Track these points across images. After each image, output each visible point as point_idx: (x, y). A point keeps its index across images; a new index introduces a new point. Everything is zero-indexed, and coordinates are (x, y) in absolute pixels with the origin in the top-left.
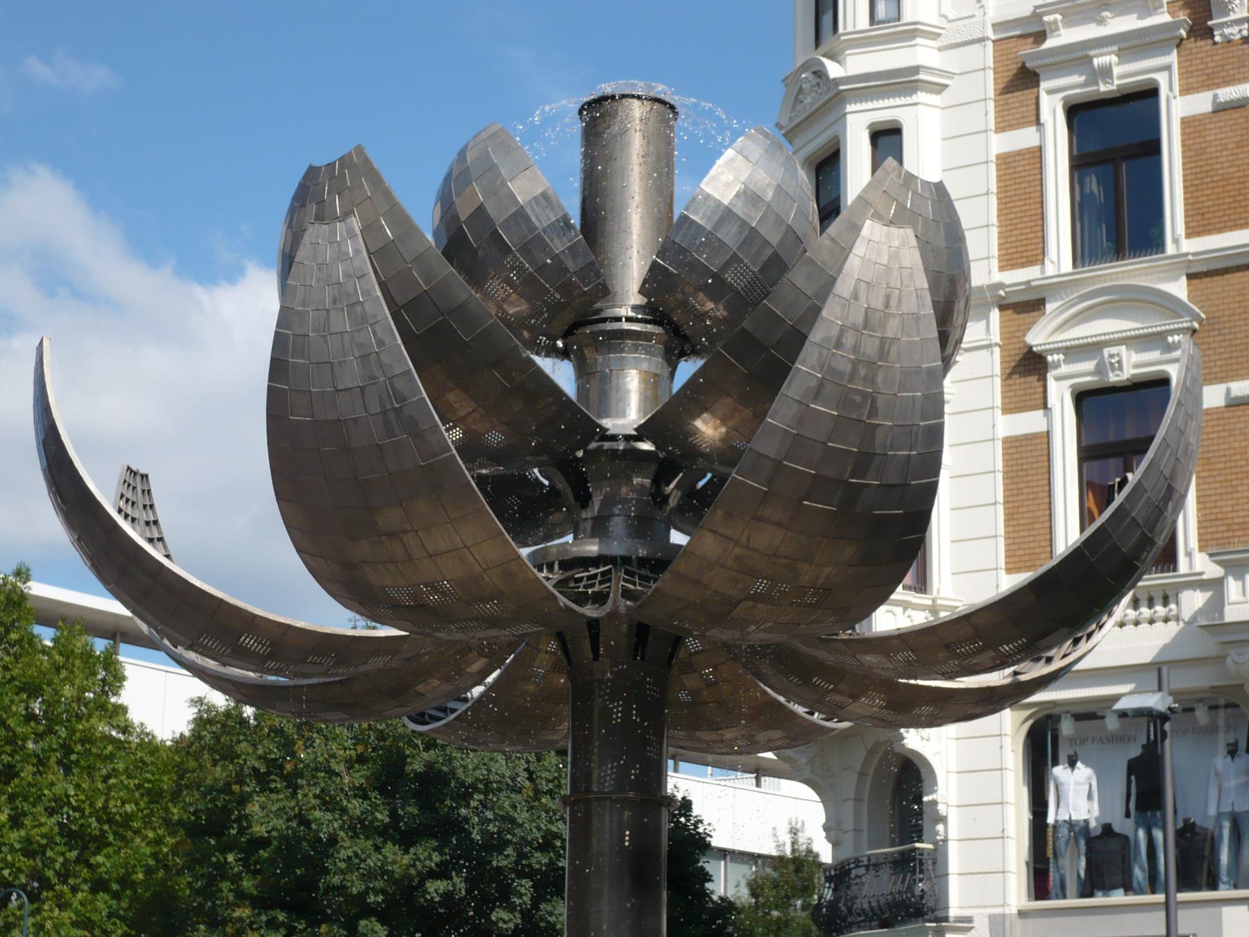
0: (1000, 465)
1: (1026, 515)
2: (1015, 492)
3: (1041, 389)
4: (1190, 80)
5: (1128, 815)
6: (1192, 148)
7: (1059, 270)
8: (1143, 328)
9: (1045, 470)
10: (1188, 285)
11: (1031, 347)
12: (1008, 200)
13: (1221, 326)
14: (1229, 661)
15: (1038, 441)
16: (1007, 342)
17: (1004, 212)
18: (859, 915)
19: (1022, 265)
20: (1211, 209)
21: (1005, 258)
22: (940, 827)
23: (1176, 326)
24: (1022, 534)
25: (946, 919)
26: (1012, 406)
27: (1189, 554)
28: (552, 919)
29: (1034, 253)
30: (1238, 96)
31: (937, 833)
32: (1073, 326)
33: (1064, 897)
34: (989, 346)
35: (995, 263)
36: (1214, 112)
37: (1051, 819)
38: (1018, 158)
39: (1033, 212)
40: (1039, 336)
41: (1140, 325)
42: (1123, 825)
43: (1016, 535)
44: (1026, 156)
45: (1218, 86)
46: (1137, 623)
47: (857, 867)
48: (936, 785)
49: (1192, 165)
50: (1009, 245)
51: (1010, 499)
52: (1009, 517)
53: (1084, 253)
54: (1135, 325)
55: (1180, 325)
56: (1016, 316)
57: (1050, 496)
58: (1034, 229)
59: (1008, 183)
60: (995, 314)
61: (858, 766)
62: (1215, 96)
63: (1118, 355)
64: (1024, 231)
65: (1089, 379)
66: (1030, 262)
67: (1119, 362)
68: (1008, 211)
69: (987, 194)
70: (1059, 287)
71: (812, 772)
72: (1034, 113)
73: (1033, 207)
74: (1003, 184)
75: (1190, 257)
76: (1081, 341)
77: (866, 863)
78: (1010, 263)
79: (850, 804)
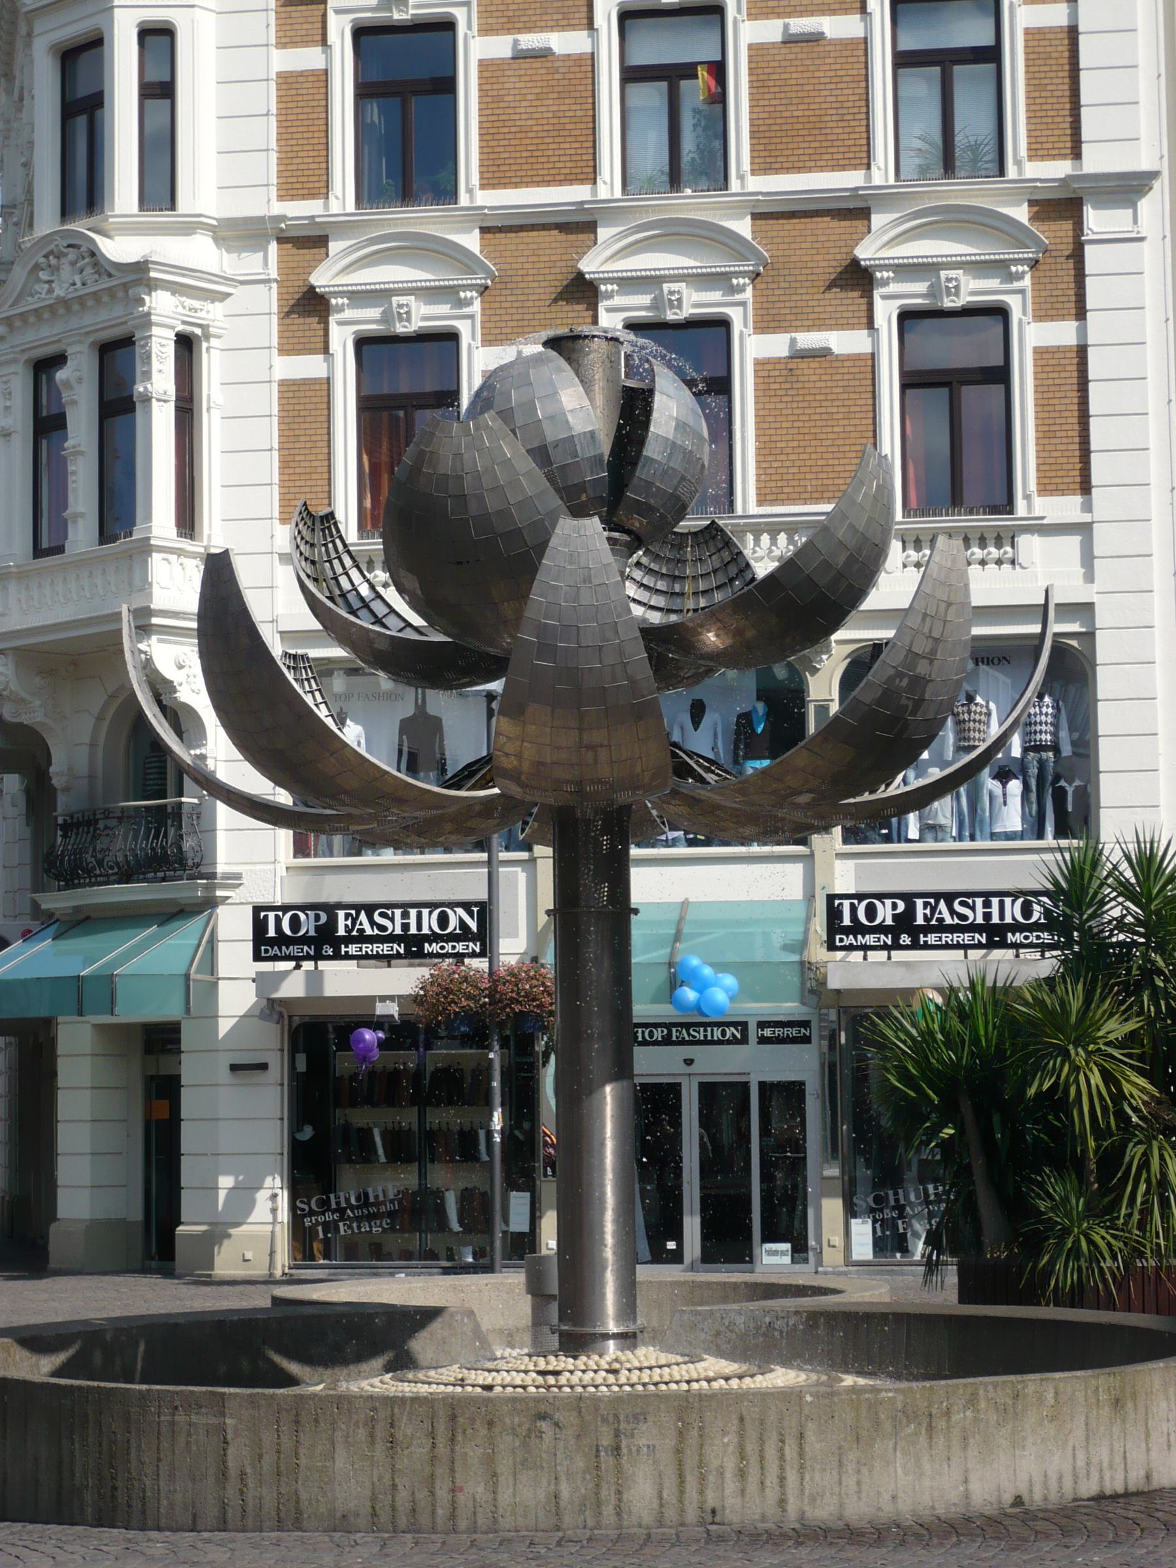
0: (275, 410)
1: (303, 464)
2: (291, 439)
3: (321, 333)
4: (490, 21)
6: (490, 93)
7: (344, 208)
8: (434, 281)
9: (324, 419)
10: (481, 239)
11: (312, 288)
12: (289, 124)
13: (514, 286)
15: (317, 387)
16: (285, 278)
17: (285, 136)
18: (111, 868)
19: (304, 197)
20: (507, 162)
21: (284, 186)
23: (469, 282)
24: (298, 483)
25: (213, 876)
26: (289, 347)
27: (1027, 497)
29: (317, 185)
30: (541, 45)
32: (897, 245)
33: (331, 855)
34: (267, 281)
35: (274, 191)
36: (513, 58)
38: (301, 79)
39: (316, 141)
40: (322, 278)
41: (433, 277)
43: (292, 484)
44: (310, 79)
45: (519, 31)
46: (983, 563)
47: (107, 818)
48: (206, 739)
49: (489, 112)
50: (289, 174)
51: (286, 446)
52: (285, 464)
53: (367, 193)
54: (693, 263)
55: (474, 282)
56: (295, 251)
57: (329, 446)
58: (317, 160)
59: (289, 105)
60: (273, 247)
61: (96, 711)
62: (516, 42)
63: (407, 305)
64: (306, 160)
65: (643, 313)
66: (311, 195)
67: (408, 313)
68: (289, 136)
69: (267, 115)
70: (344, 227)
71: (45, 715)
72: (320, 31)
73: (316, 135)
74: (284, 105)
75: (486, 211)
76: (639, 274)
77: (119, 814)
78: (291, 192)
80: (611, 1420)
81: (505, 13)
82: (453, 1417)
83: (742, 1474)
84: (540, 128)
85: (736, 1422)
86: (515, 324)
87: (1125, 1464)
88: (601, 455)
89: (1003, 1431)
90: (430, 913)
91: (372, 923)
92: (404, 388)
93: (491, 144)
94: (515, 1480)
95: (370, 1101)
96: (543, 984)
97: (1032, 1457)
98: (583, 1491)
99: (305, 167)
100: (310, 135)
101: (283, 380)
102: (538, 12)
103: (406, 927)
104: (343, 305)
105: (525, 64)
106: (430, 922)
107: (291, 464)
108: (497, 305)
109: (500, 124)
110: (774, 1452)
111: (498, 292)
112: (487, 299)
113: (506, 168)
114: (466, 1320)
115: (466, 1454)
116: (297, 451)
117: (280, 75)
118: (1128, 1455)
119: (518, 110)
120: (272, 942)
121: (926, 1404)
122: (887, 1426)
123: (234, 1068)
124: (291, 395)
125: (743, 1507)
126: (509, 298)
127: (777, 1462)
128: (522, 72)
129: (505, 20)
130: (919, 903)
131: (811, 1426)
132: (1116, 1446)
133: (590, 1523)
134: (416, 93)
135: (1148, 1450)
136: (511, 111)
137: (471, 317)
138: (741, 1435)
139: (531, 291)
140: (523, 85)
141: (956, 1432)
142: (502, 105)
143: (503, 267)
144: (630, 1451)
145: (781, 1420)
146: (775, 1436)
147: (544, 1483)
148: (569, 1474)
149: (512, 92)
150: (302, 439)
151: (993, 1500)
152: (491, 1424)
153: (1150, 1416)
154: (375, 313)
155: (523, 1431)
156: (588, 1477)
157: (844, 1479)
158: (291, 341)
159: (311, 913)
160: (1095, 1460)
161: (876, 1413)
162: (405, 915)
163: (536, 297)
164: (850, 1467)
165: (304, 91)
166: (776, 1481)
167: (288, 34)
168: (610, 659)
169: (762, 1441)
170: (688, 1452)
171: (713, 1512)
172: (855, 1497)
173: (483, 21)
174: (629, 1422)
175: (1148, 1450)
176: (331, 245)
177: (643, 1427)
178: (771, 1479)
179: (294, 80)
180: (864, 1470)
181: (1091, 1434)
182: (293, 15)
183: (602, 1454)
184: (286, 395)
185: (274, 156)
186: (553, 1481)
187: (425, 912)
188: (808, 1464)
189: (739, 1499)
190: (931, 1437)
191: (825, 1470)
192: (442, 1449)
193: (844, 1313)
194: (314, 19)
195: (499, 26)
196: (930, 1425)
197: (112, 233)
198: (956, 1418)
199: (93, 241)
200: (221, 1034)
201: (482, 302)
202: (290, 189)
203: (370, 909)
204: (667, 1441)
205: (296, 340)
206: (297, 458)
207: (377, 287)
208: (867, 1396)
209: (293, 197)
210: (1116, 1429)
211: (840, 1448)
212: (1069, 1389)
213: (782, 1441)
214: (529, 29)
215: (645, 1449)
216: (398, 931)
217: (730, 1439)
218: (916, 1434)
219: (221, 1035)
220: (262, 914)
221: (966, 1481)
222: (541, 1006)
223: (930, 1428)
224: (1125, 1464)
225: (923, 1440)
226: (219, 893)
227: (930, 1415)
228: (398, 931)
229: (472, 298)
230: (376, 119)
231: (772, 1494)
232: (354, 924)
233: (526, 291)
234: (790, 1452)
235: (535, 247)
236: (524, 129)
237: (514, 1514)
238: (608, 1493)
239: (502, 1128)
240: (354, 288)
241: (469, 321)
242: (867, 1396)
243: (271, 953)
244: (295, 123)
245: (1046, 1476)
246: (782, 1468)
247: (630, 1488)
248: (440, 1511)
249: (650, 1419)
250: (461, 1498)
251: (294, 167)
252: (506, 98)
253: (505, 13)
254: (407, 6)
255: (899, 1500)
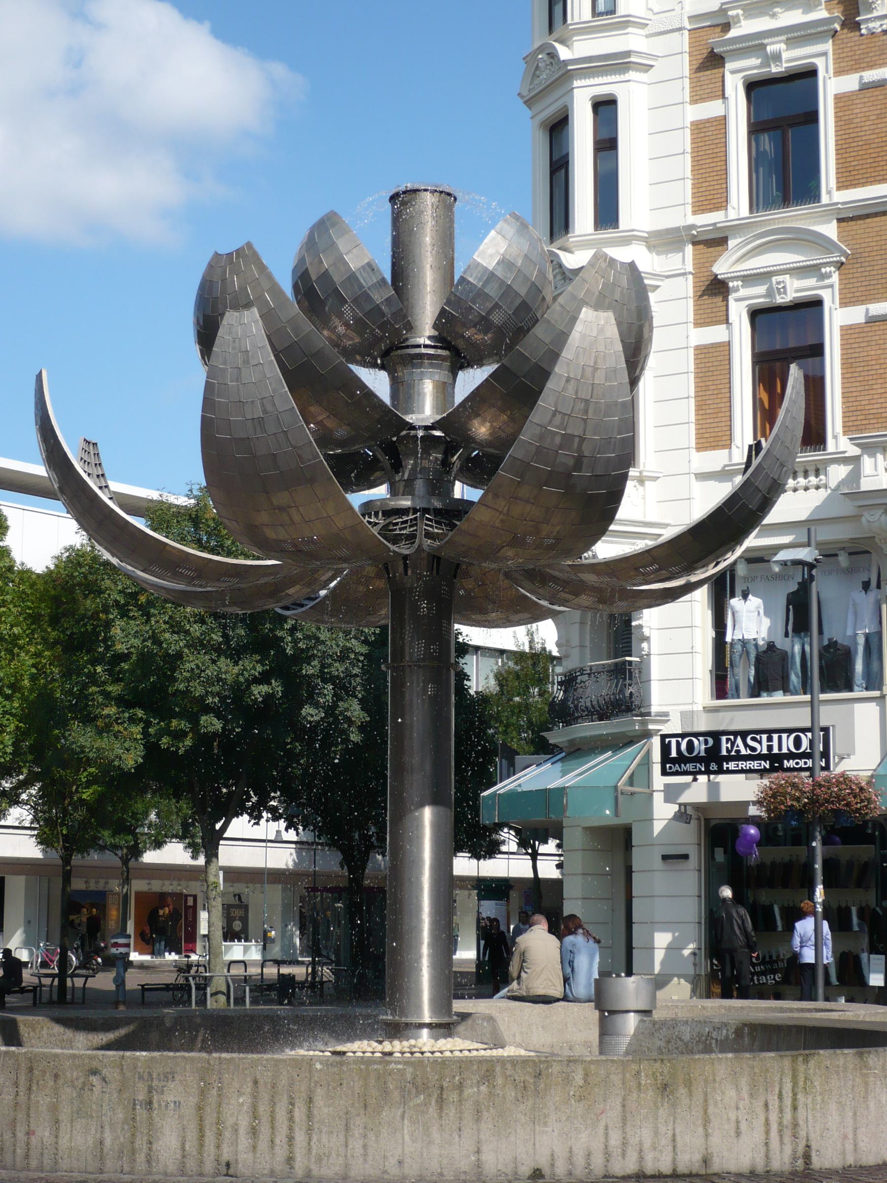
0: (692, 368)
1: (712, 406)
2: (704, 389)
4: (842, 65)
5: (787, 635)
12: (699, 158)
14: (863, 520)
15: (722, 349)
17: (697, 168)
18: (583, 711)
19: (711, 210)
22: (645, 645)
24: (708, 421)
25: (649, 714)
26: (701, 322)
28: (349, 714)
29: (719, 200)
31: (642, 650)
33: (738, 697)
34: (684, 274)
35: (689, 208)
36: (860, 90)
37: (728, 639)
38: (707, 125)
39: (719, 168)
40: (722, 268)
42: (782, 643)
44: (714, 124)
45: (864, 69)
47: (582, 674)
49: (843, 132)
50: (700, 194)
52: (700, 407)
55: (831, 260)
58: (719, 182)
59: (700, 144)
60: (689, 248)
63: (783, 282)
66: (717, 208)
67: (784, 287)
69: (683, 153)
70: (738, 228)
73: (719, 164)
75: (840, 206)
77: (589, 672)
79: (577, 626)
80: (146, 1077)
81: (853, 58)
82: (31, 1070)
83: (254, 1132)
84: (880, 140)
85: (250, 1084)
86: (864, 289)
87: (674, 1147)
88: (383, 280)
89: (522, 1107)
90: (788, 737)
91: (746, 745)
92: (792, 344)
93: (844, 156)
94: (72, 1127)
95: (771, 885)
96: (851, 788)
97: (556, 1134)
98: (122, 1139)
99: (711, 188)
100: (715, 164)
101: (697, 346)
102: (877, 53)
103: (770, 748)
104: (738, 286)
105: (868, 93)
106: (788, 744)
107: (704, 407)
108: (851, 276)
109: (851, 140)
110: (284, 1113)
111: (851, 266)
112: (843, 272)
113: (856, 173)
114: (485, 1024)
115: (38, 1102)
116: (707, 397)
117: (692, 123)
118: (678, 1138)
119: (864, 129)
120: (674, 761)
121: (436, 1077)
122: (396, 1095)
123: (665, 858)
124: (703, 356)
125: (254, 1163)
126: (859, 270)
127: (286, 1123)
128: (866, 100)
129: (853, 62)
130: (724, 738)
131: (320, 1092)
132: (662, 1129)
133: (126, 1168)
134: (792, 125)
135: (707, 1135)
136: (858, 130)
137: (831, 286)
138: (255, 1096)
139: (875, 263)
140: (866, 109)
141: (468, 1106)
142: (852, 126)
143: (855, 247)
144: (160, 1105)
145: (291, 1085)
146: (285, 1099)
147: (93, 1131)
148: (111, 1125)
149: (859, 115)
150: (711, 387)
151: (509, 1171)
152: (56, 1076)
153: (711, 1102)
154: (761, 289)
155: (79, 1083)
156: (126, 1127)
157: (350, 1142)
158: (703, 316)
159: (701, 738)
160: (633, 1141)
161: (385, 1083)
162: (770, 739)
163: (879, 267)
164: (357, 1132)
165: (710, 133)
166: (285, 1140)
167: (698, 93)
168: (272, 429)
169: (273, 1103)
170: (208, 1109)
171: (228, 1165)
172: (361, 1159)
173: (837, 65)
174: (160, 1080)
175: (707, 1135)
176: (730, 242)
177: (171, 1085)
178: (281, 1138)
179: (702, 126)
180: (371, 1136)
181: (628, 1115)
182: (702, 79)
183: (138, 1107)
184: (700, 356)
185: (689, 183)
186: (100, 1129)
187: (784, 736)
188: (316, 1126)
189: (251, 1154)
190: (441, 1108)
191: (332, 1132)
192: (22, 1098)
193: (796, 1027)
194: (717, 80)
195: (849, 68)
196: (441, 1096)
197: (573, 249)
198: (469, 1091)
199: (557, 256)
200: (656, 833)
201: (839, 274)
202: (700, 207)
203: (744, 734)
204: (191, 1098)
205: (706, 316)
206: (708, 402)
207: (762, 270)
208: (376, 1066)
209: (703, 211)
210: (663, 1113)
211: (347, 1113)
212: (602, 1072)
213: (293, 1104)
214: (871, 66)
215: (172, 1105)
216: (765, 751)
217: (245, 1099)
218: (426, 1104)
219: (656, 833)
220: (667, 740)
221: (478, 1152)
222: (848, 804)
223: (441, 1101)
224: (674, 1147)
225: (432, 1110)
226: (651, 727)
227: (442, 1088)
228: (765, 751)
229: (830, 272)
230: (767, 147)
231: (281, 1152)
232: (732, 746)
233: (872, 263)
234: (299, 1113)
235: (878, 229)
236: (868, 142)
237: (70, 1157)
238: (141, 1142)
239: (824, 901)
240: (745, 273)
241: (830, 290)
242: (376, 1066)
243: (674, 770)
244: (703, 157)
245: (571, 1152)
246: (291, 1129)
247: (158, 1139)
248: (18, 1151)
249: (178, 1078)
250: (34, 1140)
251: (704, 189)
252: (855, 121)
253: (853, 58)
254: (781, 61)
255: (406, 1165)
